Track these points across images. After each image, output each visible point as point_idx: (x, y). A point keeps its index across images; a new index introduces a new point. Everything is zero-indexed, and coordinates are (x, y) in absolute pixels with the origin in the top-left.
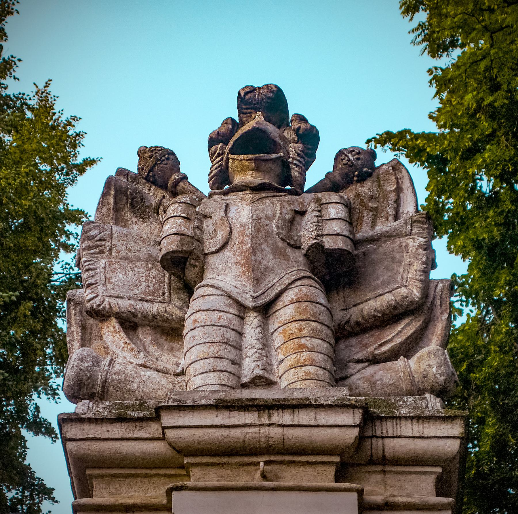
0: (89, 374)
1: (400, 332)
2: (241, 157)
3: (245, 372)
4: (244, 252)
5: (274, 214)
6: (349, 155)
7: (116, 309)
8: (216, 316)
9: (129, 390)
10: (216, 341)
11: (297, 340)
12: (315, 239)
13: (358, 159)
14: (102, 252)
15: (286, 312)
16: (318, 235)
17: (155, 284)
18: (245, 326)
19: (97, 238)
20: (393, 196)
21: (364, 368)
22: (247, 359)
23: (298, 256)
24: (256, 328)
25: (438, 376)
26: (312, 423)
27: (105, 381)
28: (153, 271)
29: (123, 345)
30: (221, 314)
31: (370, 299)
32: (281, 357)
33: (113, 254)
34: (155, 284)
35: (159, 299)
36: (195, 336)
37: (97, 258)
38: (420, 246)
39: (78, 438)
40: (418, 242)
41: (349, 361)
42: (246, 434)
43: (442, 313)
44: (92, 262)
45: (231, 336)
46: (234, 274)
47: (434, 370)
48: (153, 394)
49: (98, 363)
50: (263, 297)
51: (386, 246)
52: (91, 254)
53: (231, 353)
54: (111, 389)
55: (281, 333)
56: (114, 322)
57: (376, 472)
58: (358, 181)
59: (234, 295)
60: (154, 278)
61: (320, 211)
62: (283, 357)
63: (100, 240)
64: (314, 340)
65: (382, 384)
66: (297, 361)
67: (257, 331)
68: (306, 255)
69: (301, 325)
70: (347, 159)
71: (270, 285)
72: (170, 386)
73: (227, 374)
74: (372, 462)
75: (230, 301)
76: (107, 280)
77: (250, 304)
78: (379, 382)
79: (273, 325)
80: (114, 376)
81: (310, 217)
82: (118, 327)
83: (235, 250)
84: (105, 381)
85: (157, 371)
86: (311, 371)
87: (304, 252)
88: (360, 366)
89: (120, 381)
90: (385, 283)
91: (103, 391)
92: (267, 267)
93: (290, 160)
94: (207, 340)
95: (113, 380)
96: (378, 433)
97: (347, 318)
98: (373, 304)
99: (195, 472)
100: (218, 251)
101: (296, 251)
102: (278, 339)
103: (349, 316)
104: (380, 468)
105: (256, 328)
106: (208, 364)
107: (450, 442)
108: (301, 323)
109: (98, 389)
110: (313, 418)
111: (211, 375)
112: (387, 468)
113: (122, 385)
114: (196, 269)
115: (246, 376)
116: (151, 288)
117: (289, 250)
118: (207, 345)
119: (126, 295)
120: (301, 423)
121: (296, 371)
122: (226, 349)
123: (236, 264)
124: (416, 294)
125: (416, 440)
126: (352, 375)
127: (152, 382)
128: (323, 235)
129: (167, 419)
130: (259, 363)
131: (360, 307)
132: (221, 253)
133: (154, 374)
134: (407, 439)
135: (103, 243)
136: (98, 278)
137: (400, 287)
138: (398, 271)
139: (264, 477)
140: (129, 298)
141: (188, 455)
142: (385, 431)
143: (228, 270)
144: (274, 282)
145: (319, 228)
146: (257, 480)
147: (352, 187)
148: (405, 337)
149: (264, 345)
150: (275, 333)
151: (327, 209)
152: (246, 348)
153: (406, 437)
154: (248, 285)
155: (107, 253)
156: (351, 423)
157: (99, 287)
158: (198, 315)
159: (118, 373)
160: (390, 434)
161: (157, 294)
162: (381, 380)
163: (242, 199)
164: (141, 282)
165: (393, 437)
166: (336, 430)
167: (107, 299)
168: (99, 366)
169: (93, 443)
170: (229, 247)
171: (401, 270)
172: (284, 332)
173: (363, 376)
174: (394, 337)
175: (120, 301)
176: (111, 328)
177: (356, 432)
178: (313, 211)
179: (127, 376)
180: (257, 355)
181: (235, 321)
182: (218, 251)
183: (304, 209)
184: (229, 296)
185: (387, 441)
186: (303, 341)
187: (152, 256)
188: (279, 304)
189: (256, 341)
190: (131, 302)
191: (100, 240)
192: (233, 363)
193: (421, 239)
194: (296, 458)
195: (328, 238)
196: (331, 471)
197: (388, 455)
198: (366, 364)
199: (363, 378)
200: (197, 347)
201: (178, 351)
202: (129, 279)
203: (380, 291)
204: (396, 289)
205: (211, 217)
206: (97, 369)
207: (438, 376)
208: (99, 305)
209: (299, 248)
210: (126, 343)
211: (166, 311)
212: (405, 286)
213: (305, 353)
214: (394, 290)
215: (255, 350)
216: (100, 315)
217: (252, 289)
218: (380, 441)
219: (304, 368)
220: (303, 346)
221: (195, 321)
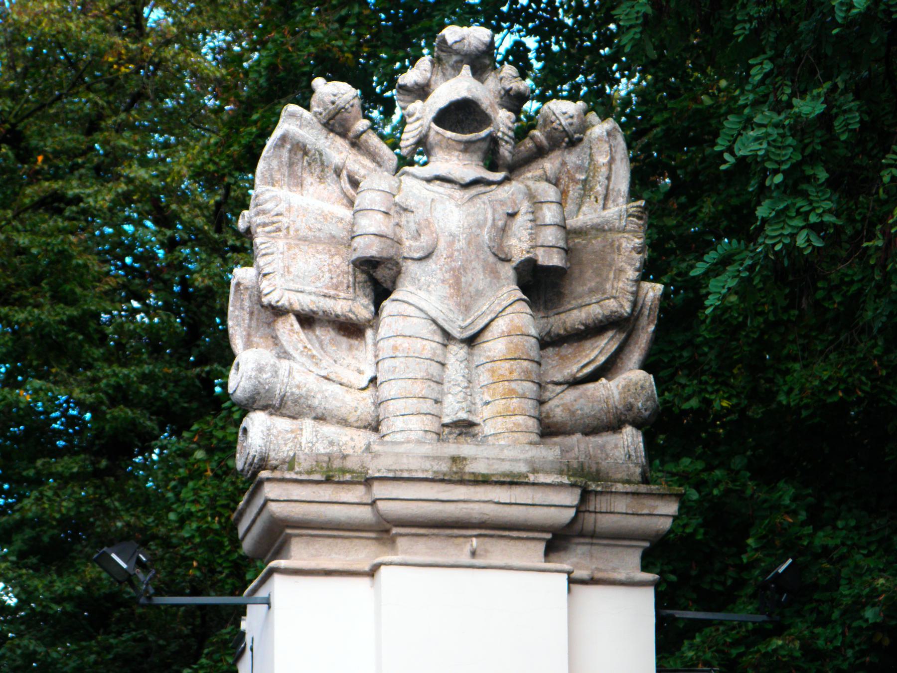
0: (267, 387)
1: (603, 348)
2: (449, 134)
3: (447, 411)
4: (452, 269)
5: (486, 219)
6: (561, 118)
7: (297, 307)
8: (419, 346)
9: (309, 406)
10: (419, 376)
11: (506, 383)
12: (528, 252)
13: (571, 124)
14: (279, 230)
15: (495, 346)
16: (532, 247)
17: (338, 276)
18: (448, 355)
19: (273, 213)
20: (604, 170)
21: (563, 391)
22: (450, 396)
23: (507, 271)
24: (461, 362)
25: (643, 411)
26: (530, 502)
27: (285, 395)
28: (336, 257)
29: (302, 349)
30: (425, 342)
31: (574, 309)
32: (487, 398)
33: (291, 232)
34: (338, 276)
35: (342, 295)
36: (395, 367)
37: (273, 238)
38: (634, 248)
39: (282, 499)
40: (633, 243)
41: (548, 383)
42: (461, 509)
43: (649, 324)
44: (268, 245)
45: (435, 369)
46: (439, 293)
47: (640, 404)
48: (335, 412)
49: (276, 372)
50: (471, 327)
51: (597, 243)
52: (269, 232)
53: (431, 390)
54: (289, 403)
55: (489, 370)
56: (292, 319)
57: (583, 544)
58: (566, 148)
59: (441, 322)
60: (338, 267)
61: (533, 213)
62: (490, 399)
63: (277, 215)
64: (524, 383)
65: (582, 414)
66: (507, 408)
67: (463, 366)
68: (516, 269)
69: (511, 366)
70: (558, 122)
71: (479, 313)
72: (354, 404)
73: (429, 417)
74: (582, 535)
75: (434, 327)
76: (287, 269)
77: (456, 333)
78: (579, 412)
79: (479, 359)
80: (294, 390)
81: (522, 220)
82: (297, 326)
83: (442, 263)
84: (285, 395)
85: (341, 384)
86: (521, 422)
87: (514, 264)
88: (559, 389)
89: (301, 397)
90: (592, 291)
91: (281, 405)
92: (477, 290)
93: (500, 134)
94: (408, 376)
95: (292, 394)
96: (592, 508)
97: (547, 330)
98: (576, 316)
99: (401, 542)
100: (420, 259)
101: (506, 264)
102: (484, 377)
103: (549, 327)
104: (587, 540)
105: (461, 362)
106: (412, 405)
107: (662, 519)
108: (512, 362)
109: (276, 402)
110: (531, 496)
111: (414, 418)
112: (595, 541)
113: (302, 400)
114: (392, 272)
115: (448, 415)
116: (335, 281)
117: (500, 265)
118: (410, 381)
119: (308, 289)
120: (518, 502)
121: (505, 420)
122: (430, 386)
123: (443, 281)
124: (627, 308)
125: (628, 516)
126: (550, 399)
127: (335, 398)
128: (537, 246)
129: (379, 490)
130: (464, 405)
131: (563, 316)
132: (424, 263)
133: (337, 387)
134: (619, 516)
135: (280, 218)
136: (276, 266)
137: (608, 299)
138: (607, 277)
139: (473, 554)
140: (310, 293)
141: (397, 526)
142: (598, 506)
143: (432, 286)
144: (483, 310)
145: (533, 237)
146: (466, 559)
147: (557, 153)
148: (609, 354)
149: (470, 382)
150: (481, 367)
151: (541, 209)
152: (449, 382)
153: (619, 513)
154: (456, 311)
155: (284, 232)
156: (568, 504)
157: (277, 277)
158: (400, 340)
159: (298, 387)
160: (604, 510)
161: (340, 288)
162: (581, 409)
163: (451, 197)
164: (323, 272)
165: (607, 513)
166: (553, 509)
167: (287, 293)
168: (277, 376)
169: (298, 504)
170: (434, 257)
171: (612, 275)
172: (493, 371)
173: (561, 402)
174: (597, 356)
175: (300, 295)
176: (288, 327)
177: (572, 513)
178: (526, 213)
179: (308, 391)
180: (462, 394)
181: (439, 349)
182: (420, 259)
183: (516, 210)
184: (434, 321)
185: (599, 516)
186: (513, 385)
187: (334, 237)
188: (488, 335)
189: (461, 378)
190: (313, 298)
191: (277, 215)
192: (436, 402)
193: (637, 241)
194: (507, 533)
195: (542, 249)
196: (541, 547)
197: (598, 530)
198: (565, 386)
199: (563, 405)
200: (399, 382)
201: (357, 349)
202: (310, 268)
203: (587, 300)
204: (605, 299)
205: (412, 212)
206: (275, 380)
207: (643, 411)
208: (278, 301)
209: (509, 261)
210: (306, 347)
211: (350, 311)
212: (615, 298)
213: (515, 400)
214: (602, 300)
215: (460, 389)
216: (278, 312)
217: (461, 318)
218: (593, 515)
219: (513, 418)
220: (512, 391)
221: (395, 348)
